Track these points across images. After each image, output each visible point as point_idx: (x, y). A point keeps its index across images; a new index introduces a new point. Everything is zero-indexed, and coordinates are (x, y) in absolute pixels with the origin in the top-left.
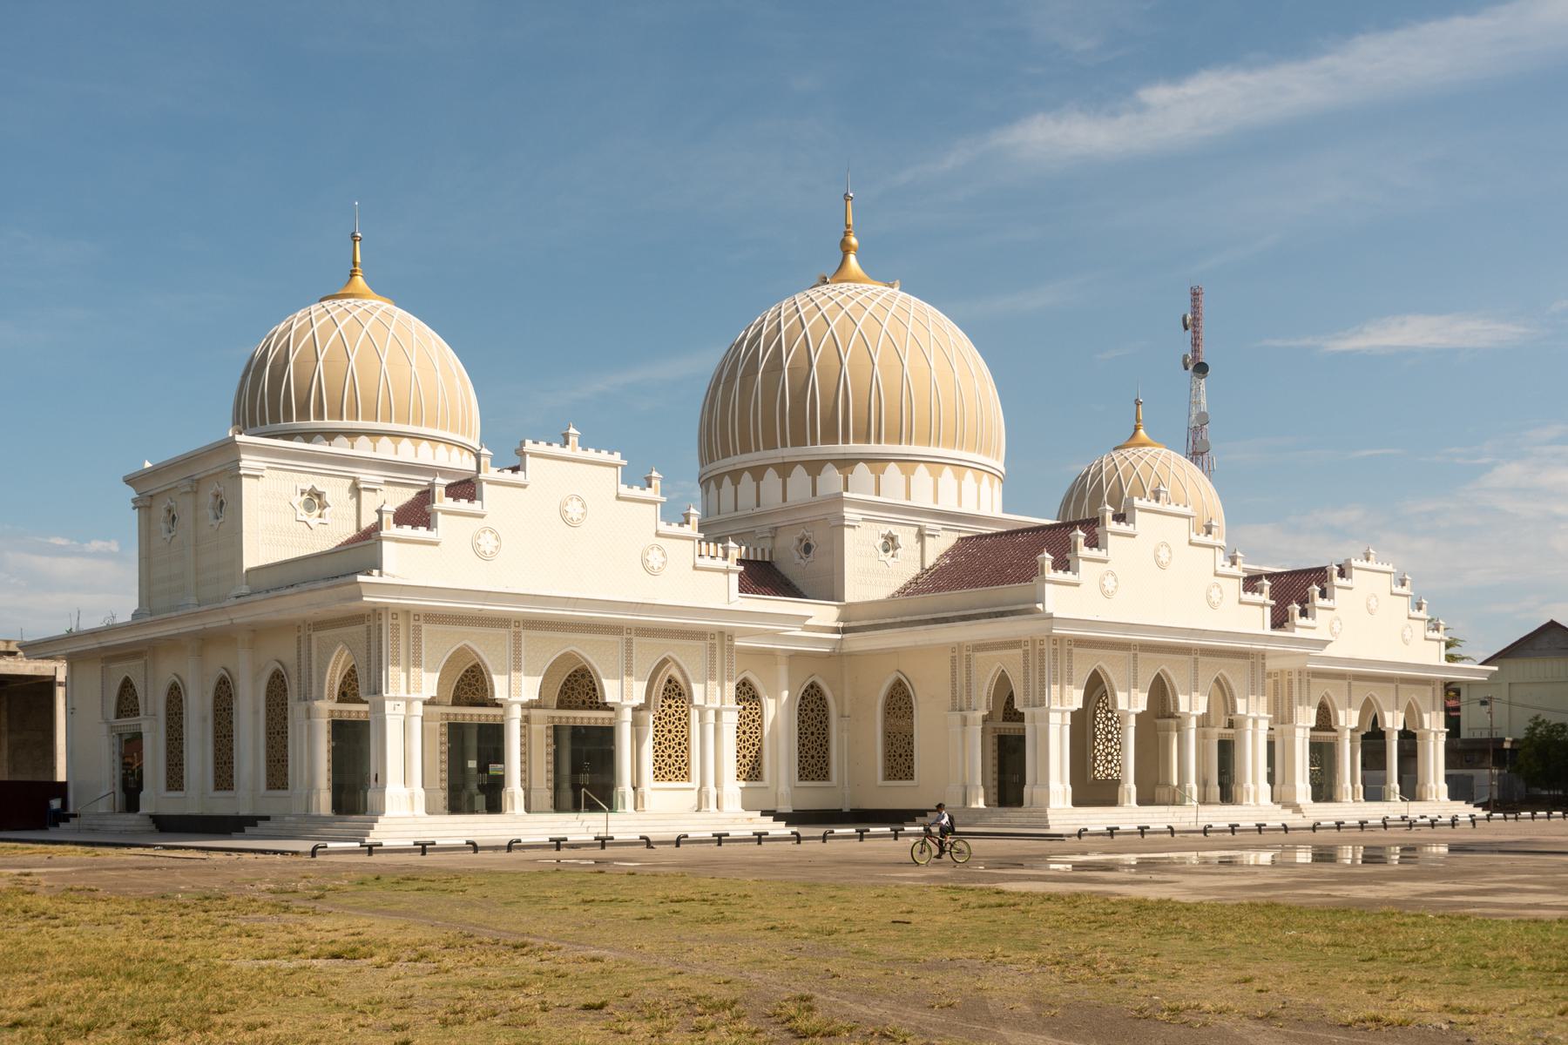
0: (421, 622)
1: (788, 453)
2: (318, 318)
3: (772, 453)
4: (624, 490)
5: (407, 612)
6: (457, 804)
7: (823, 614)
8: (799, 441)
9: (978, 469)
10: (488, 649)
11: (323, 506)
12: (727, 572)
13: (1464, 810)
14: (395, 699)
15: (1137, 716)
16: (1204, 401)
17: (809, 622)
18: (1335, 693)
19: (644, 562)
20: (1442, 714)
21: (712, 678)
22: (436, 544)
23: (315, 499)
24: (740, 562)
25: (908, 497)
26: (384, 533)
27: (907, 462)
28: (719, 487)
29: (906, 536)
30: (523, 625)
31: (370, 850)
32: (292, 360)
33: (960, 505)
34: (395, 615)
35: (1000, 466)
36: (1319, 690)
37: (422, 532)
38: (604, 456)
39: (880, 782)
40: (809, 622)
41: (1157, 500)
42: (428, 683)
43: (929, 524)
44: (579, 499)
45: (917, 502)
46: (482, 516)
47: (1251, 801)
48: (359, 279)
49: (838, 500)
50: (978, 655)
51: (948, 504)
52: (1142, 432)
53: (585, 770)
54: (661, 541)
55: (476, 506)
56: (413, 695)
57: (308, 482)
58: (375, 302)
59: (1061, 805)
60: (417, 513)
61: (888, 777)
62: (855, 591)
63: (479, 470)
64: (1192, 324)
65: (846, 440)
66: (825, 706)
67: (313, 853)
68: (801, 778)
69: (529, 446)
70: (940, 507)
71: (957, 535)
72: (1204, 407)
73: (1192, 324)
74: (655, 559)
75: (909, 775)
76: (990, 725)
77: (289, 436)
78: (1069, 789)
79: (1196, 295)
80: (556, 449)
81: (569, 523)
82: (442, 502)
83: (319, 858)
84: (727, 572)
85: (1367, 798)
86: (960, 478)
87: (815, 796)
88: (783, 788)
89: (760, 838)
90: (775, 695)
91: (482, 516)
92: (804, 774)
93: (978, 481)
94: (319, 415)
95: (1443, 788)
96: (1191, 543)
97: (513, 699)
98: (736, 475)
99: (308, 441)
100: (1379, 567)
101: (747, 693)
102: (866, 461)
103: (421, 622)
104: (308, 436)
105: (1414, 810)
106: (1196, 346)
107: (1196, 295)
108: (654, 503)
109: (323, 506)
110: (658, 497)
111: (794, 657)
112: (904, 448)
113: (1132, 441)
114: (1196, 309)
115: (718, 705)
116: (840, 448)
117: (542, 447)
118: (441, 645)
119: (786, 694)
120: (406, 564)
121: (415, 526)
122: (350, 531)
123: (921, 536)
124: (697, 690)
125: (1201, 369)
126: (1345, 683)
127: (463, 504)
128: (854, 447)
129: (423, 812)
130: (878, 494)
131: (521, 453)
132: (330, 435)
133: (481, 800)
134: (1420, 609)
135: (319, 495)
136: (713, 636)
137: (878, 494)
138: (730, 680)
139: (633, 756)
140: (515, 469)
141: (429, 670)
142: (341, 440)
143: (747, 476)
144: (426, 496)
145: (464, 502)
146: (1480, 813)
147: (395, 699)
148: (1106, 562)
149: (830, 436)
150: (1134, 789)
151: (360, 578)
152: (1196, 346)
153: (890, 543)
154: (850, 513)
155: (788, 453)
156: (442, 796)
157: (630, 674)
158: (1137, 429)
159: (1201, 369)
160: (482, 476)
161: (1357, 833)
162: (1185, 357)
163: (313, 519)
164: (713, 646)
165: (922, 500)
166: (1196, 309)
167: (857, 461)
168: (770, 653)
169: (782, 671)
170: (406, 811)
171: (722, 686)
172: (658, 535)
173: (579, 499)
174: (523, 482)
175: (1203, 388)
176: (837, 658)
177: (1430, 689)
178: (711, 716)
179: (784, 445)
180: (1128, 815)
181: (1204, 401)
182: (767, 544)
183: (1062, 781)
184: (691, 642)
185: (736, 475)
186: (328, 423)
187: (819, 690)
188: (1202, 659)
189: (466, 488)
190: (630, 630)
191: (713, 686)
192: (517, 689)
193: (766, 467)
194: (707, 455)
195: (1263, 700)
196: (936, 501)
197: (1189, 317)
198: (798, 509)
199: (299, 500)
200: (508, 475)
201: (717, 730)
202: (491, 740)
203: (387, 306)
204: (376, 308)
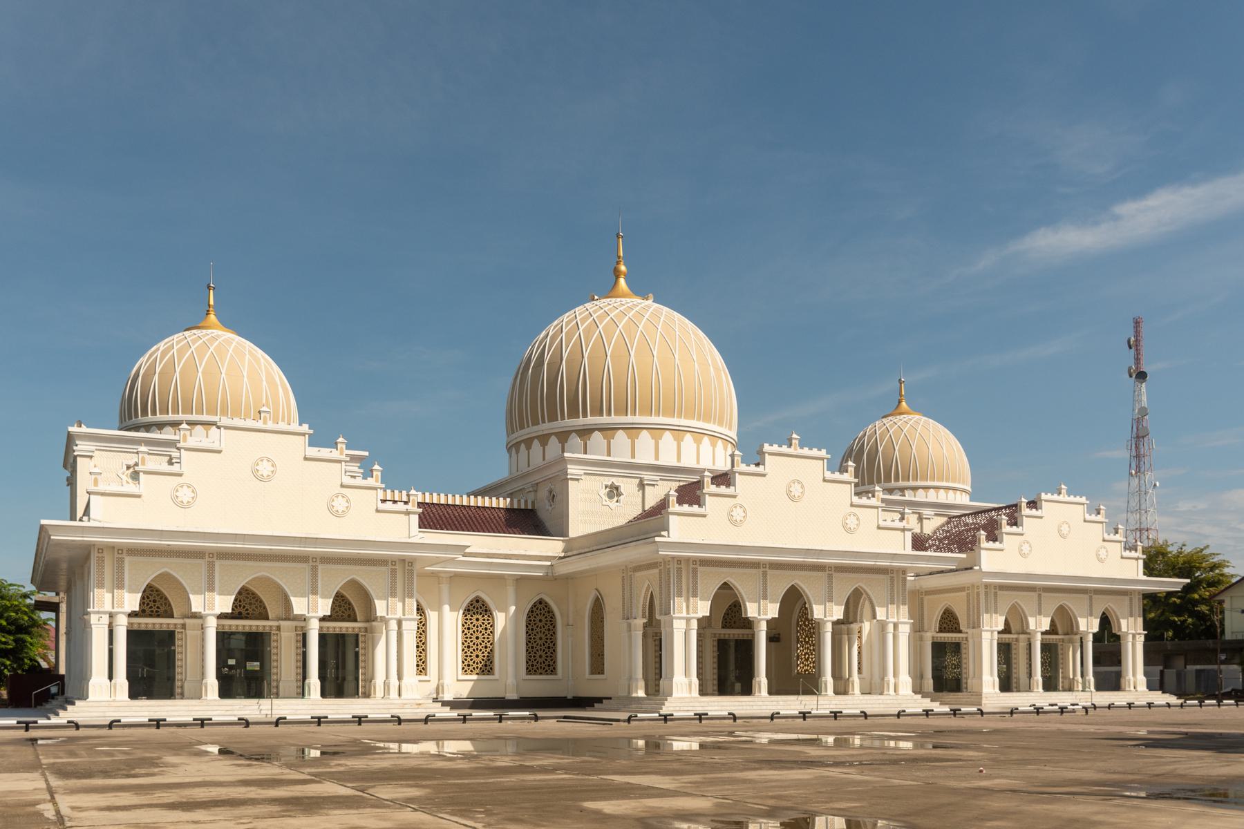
0: (124, 555)
1: (546, 427)
2: (178, 343)
3: (536, 428)
4: (828, 475)
5: (112, 547)
6: (723, 688)
7: (549, 547)
8: (553, 418)
9: (714, 437)
10: (744, 586)
11: (619, 494)
12: (408, 513)
13: (1160, 698)
14: (98, 612)
15: (699, 620)
16: (1144, 398)
17: (468, 550)
18: (1026, 603)
19: (844, 525)
20: (1140, 620)
21: (393, 595)
22: (704, 516)
23: (614, 492)
24: (420, 505)
25: (633, 456)
26: (671, 509)
27: (633, 429)
28: (517, 452)
29: (628, 487)
30: (211, 556)
31: (666, 718)
32: (158, 370)
33: (698, 462)
34: (101, 550)
35: (733, 434)
36: (1006, 601)
37: (695, 509)
38: (815, 452)
39: (587, 675)
40: (468, 550)
41: (790, 446)
42: (703, 608)
43: (648, 476)
44: (799, 482)
45: (641, 459)
46: (180, 475)
47: (892, 692)
48: (212, 317)
49: (563, 461)
50: (638, 574)
51: (668, 459)
52: (904, 404)
53: (342, 667)
54: (344, 491)
55: (731, 490)
56: (116, 610)
57: (609, 481)
58: (220, 333)
59: (991, 690)
60: (691, 494)
61: (592, 673)
62: (578, 526)
63: (733, 466)
64: (1135, 345)
65: (585, 415)
66: (553, 617)
67: (629, 720)
68: (529, 672)
69: (767, 447)
70: (662, 462)
71: (677, 484)
72: (1144, 402)
73: (1135, 345)
74: (852, 522)
75: (602, 672)
76: (708, 632)
77: (136, 428)
78: (997, 680)
79: (1137, 323)
80: (785, 449)
81: (793, 499)
82: (710, 488)
83: (633, 723)
84: (408, 513)
85: (1100, 687)
86: (698, 442)
87: (540, 686)
88: (511, 680)
89: (927, 713)
90: (504, 609)
91: (180, 475)
92: (532, 668)
93: (714, 445)
94: (154, 413)
95: (1141, 679)
96: (825, 480)
97: (207, 612)
98: (528, 442)
99: (147, 431)
100: (1067, 499)
101: (477, 609)
102: (600, 430)
103: (124, 555)
104: (148, 427)
105: (874, 704)
106: (1137, 360)
107: (1137, 323)
108: (850, 483)
109: (619, 494)
110: (853, 479)
111: (519, 580)
112: (629, 419)
113: (896, 411)
114: (1137, 333)
115: (399, 615)
116: (581, 421)
117: (775, 448)
118: (711, 583)
119: (513, 608)
120: (683, 529)
121: (691, 504)
122: (638, 511)
123: (642, 486)
124: (380, 608)
125: (1142, 376)
126: (1035, 595)
127: (723, 489)
128: (591, 420)
129: (1145, 688)
130: (609, 455)
131: (761, 453)
132: (160, 426)
133: (738, 686)
134: (1117, 533)
135: (617, 488)
136: (394, 563)
137: (609, 455)
138: (411, 596)
139: (382, 658)
140: (757, 465)
141: (131, 591)
142: (168, 429)
143: (536, 442)
144: (698, 485)
145: (723, 487)
146: (1173, 700)
147: (98, 612)
148: (735, 497)
149: (574, 413)
150: (1040, 680)
151: (657, 539)
152: (1137, 360)
153: (614, 492)
154: (573, 470)
155: (546, 427)
156: (712, 682)
157: (765, 598)
158: (900, 402)
159: (1142, 376)
160: (736, 469)
161: (832, 723)
162: (1130, 369)
163: (613, 503)
164: (393, 572)
165: (645, 456)
166: (1137, 333)
167: (570, 432)
168: (501, 577)
169: (510, 591)
170: (105, 697)
171: (898, 608)
172: (852, 505)
173: (799, 482)
174: (216, 446)
175: (1144, 390)
176: (551, 578)
177: (1127, 598)
178: (890, 628)
179: (544, 422)
180: (761, 702)
181: (1144, 398)
182: (531, 497)
183: (992, 674)
184: (358, 567)
185: (528, 442)
186: (160, 417)
187: (547, 605)
188: (835, 575)
189: (723, 479)
190: (830, 569)
191: (892, 608)
192: (762, 611)
193: (550, 435)
194: (511, 429)
195: (904, 610)
196: (657, 458)
197: (1133, 339)
198: (539, 470)
199: (604, 492)
200: (753, 468)
201: (895, 637)
202: (746, 648)
203: (229, 335)
204: (219, 336)
